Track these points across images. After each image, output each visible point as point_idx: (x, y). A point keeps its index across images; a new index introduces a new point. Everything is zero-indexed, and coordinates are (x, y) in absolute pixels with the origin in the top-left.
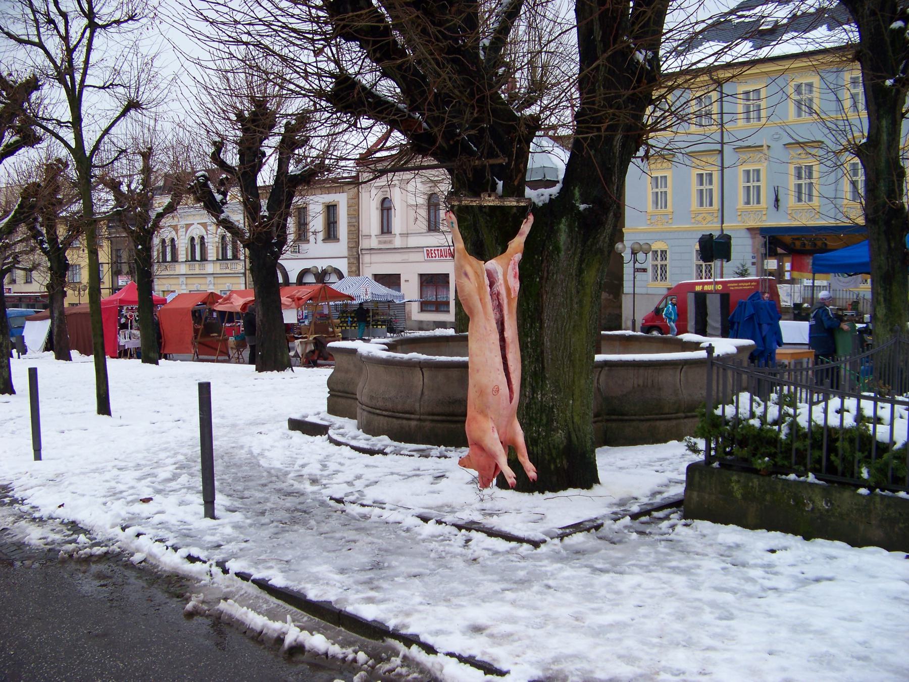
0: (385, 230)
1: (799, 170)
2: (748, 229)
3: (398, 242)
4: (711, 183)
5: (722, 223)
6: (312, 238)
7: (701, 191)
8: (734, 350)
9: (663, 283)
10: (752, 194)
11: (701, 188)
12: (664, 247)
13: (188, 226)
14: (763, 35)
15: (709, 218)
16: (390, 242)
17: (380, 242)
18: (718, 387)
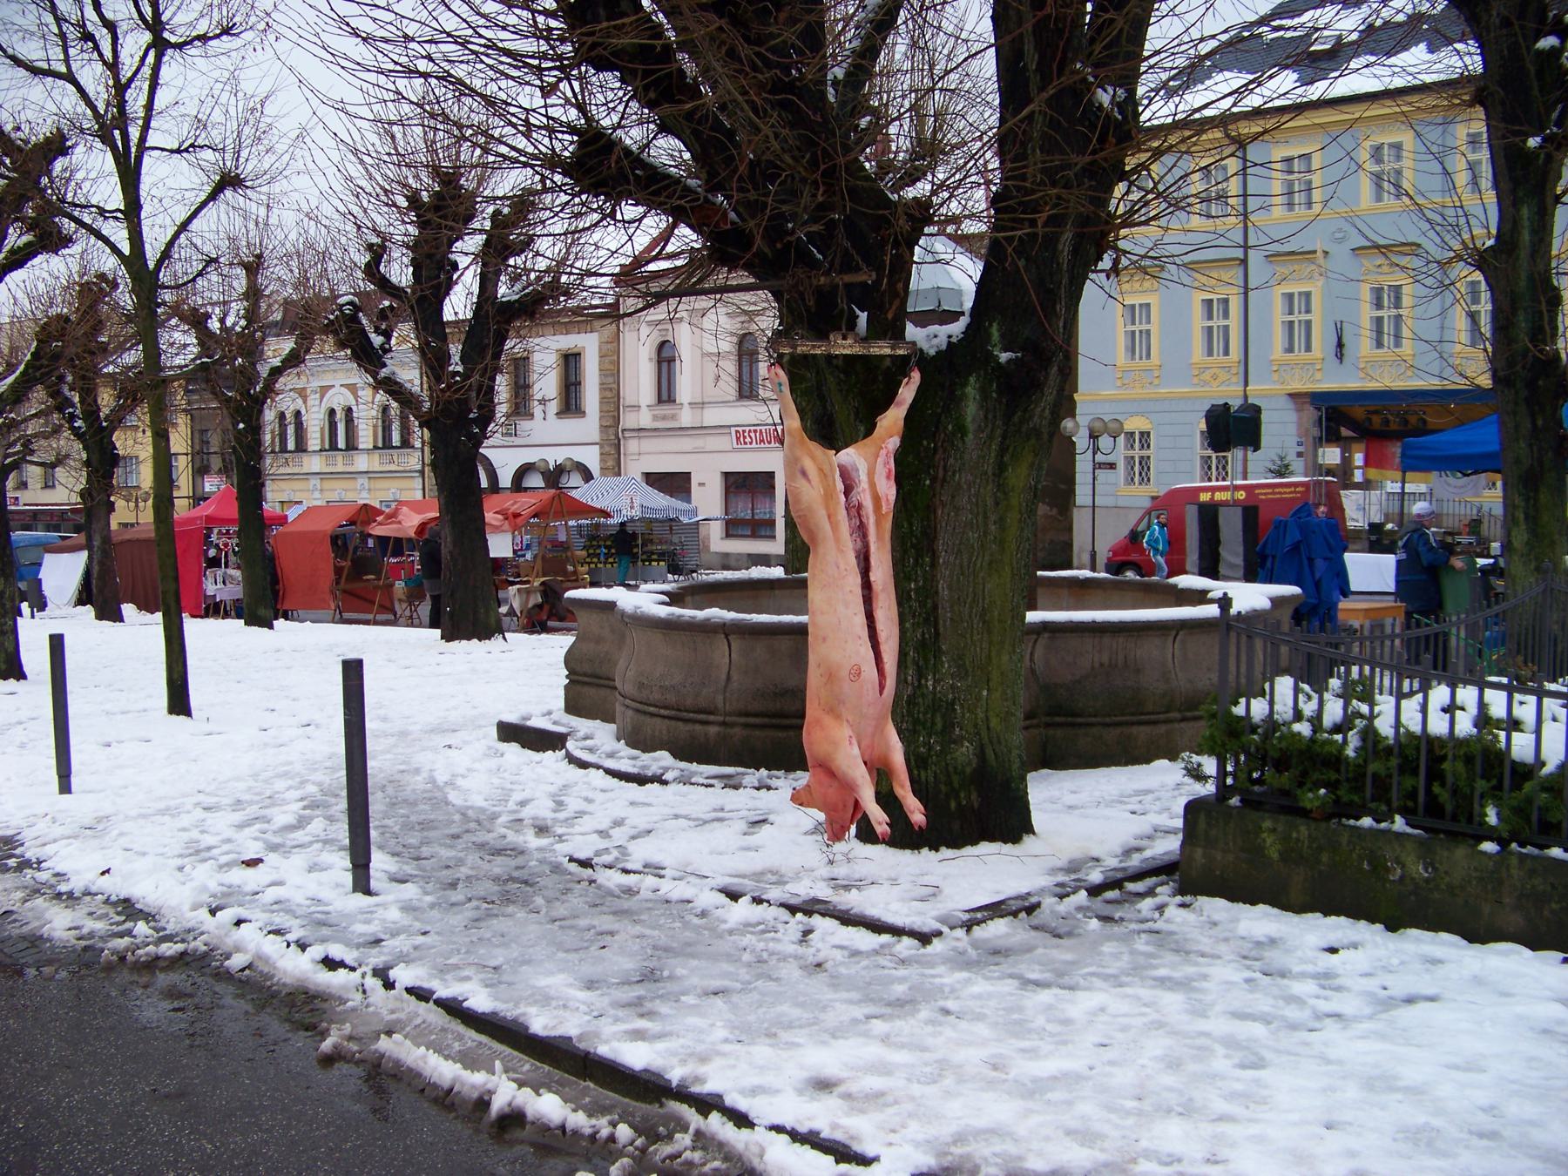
0: (665, 397)
1: (1378, 292)
2: (1290, 395)
3: (686, 418)
4: (1226, 315)
5: (1246, 384)
6: (537, 410)
7: (1210, 329)
8: (1266, 604)
9: (1143, 488)
10: (1297, 335)
11: (1210, 323)
12: (1145, 427)
13: (324, 390)
14: (1317, 61)
15: (1223, 376)
16: (673, 417)
17: (655, 418)
18: (1238, 667)
